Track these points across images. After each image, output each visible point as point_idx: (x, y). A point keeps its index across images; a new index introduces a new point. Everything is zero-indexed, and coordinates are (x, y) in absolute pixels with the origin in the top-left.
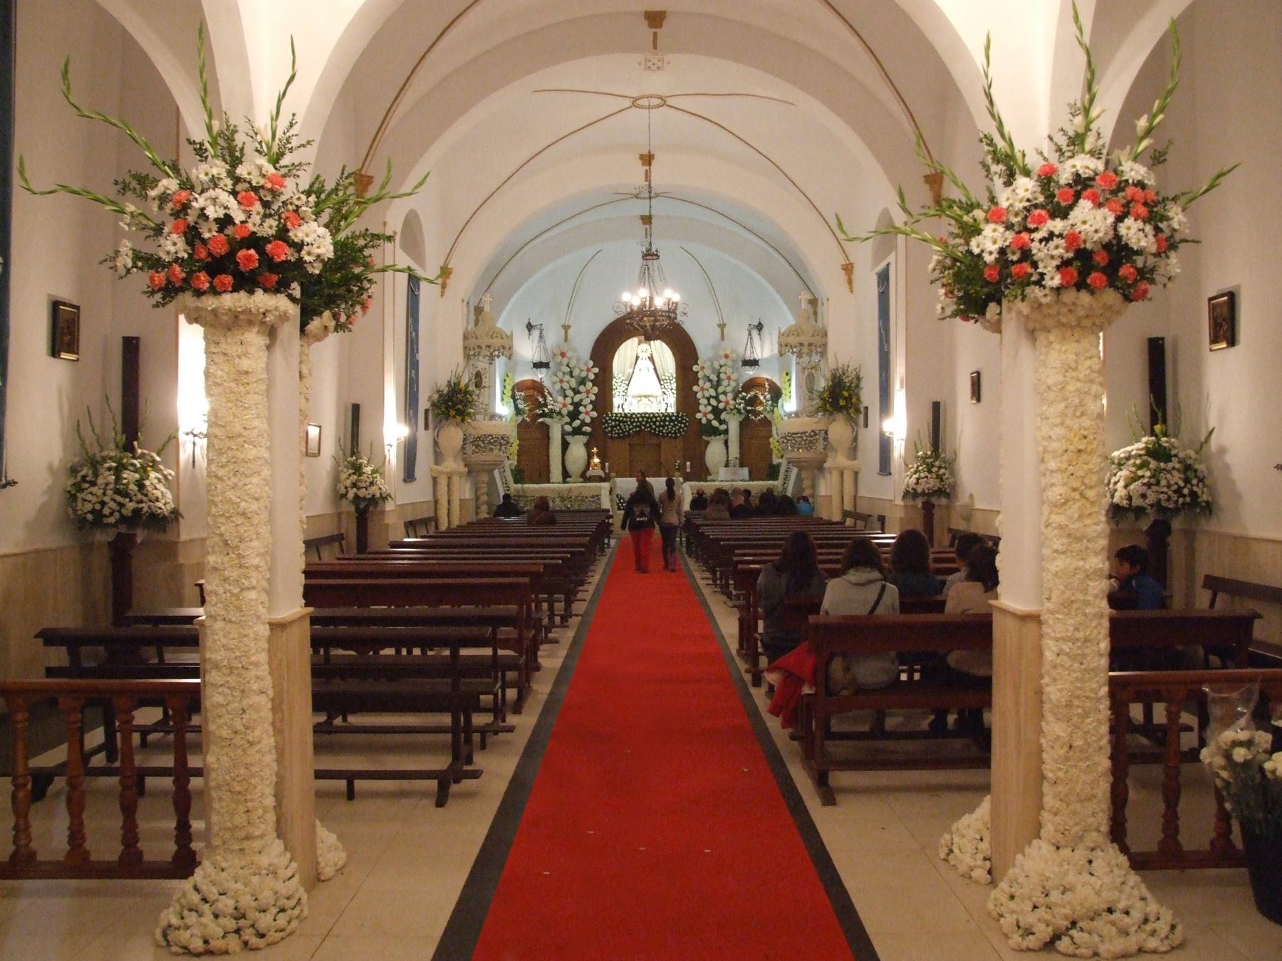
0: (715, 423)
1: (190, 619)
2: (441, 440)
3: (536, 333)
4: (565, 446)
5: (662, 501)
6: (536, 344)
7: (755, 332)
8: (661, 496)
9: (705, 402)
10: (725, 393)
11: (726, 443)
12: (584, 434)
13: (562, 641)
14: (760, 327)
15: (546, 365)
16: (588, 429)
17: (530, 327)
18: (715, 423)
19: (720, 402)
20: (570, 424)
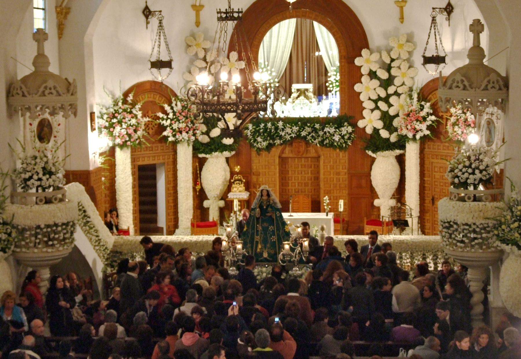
0: (384, 134)
1: (49, 141)
2: (399, 85)
3: (154, 21)
4: (199, 165)
5: (461, 273)
6: (155, 37)
7: (441, 18)
8: (381, 241)
9: (372, 105)
10: (396, 94)
11: (401, 160)
12: (225, 148)
13: (44, 196)
14: (449, 9)
15: (168, 64)
16: (228, 141)
17: (147, 13)
18: (384, 134)
19: (390, 105)
20: (207, 133)
